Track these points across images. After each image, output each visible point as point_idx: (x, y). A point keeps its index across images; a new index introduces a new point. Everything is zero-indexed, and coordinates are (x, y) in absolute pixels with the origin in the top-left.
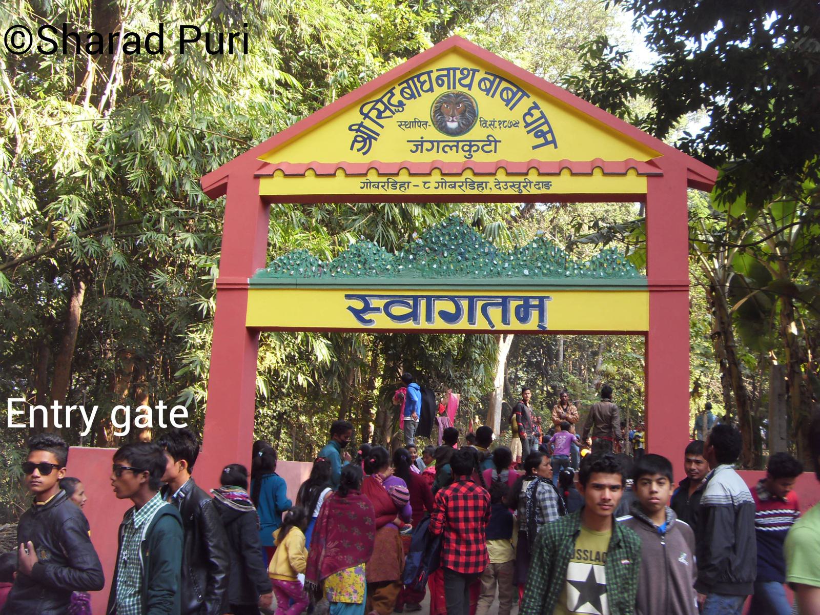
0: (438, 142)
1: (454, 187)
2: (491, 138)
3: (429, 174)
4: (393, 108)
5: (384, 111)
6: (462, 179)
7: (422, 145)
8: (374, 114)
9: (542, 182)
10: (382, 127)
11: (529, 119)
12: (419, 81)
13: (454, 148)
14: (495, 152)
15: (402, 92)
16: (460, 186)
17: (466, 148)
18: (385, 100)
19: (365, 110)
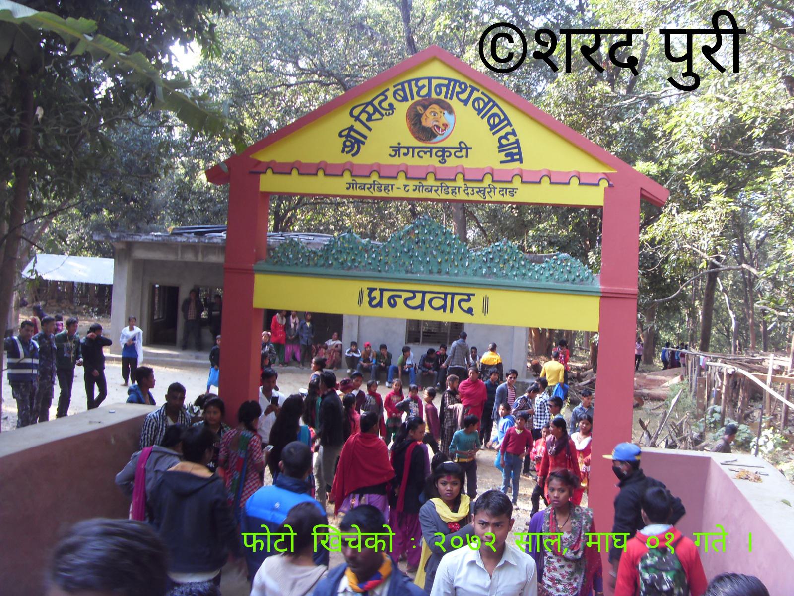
0: (414, 148)
1: (364, 189)
2: (463, 145)
3: (396, 178)
4: (383, 112)
5: (374, 113)
6: (370, 181)
7: (399, 151)
8: (364, 117)
9: (506, 189)
10: (370, 129)
11: (504, 141)
12: (417, 85)
13: (428, 154)
14: (467, 157)
15: (395, 93)
16: (368, 189)
17: (440, 154)
18: (376, 103)
19: (356, 112)
